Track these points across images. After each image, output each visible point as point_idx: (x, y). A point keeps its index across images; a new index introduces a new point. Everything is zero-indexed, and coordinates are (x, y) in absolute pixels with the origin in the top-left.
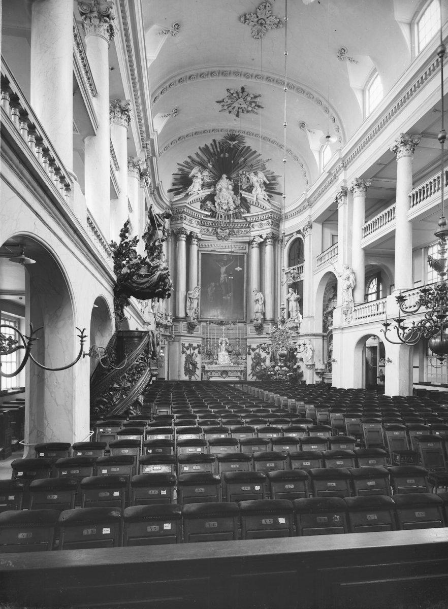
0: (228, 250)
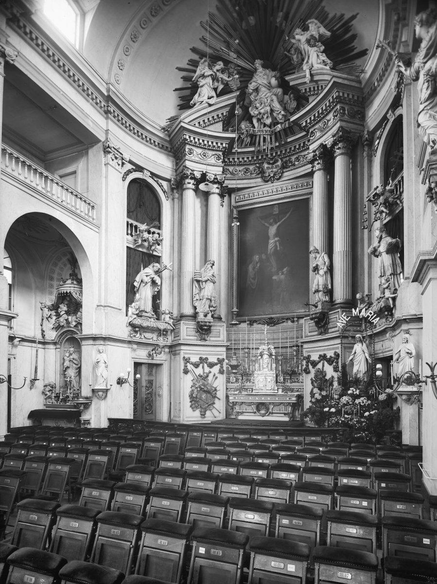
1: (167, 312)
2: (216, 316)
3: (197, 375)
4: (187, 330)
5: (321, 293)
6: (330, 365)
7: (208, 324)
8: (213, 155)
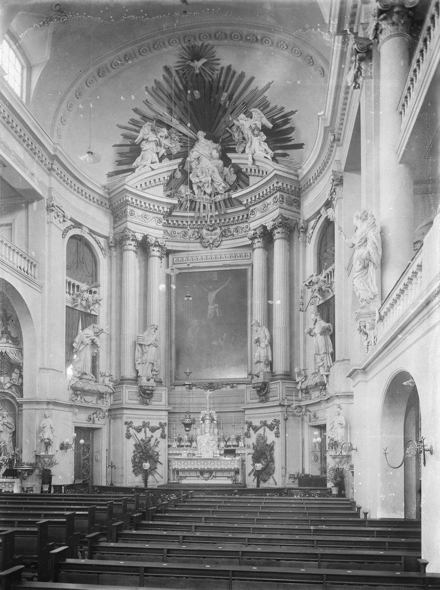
0: (220, 264)
1: (108, 374)
2: (157, 380)
3: (140, 439)
4: (129, 394)
5: (262, 364)
6: (272, 430)
7: (151, 388)
8: (154, 218)
